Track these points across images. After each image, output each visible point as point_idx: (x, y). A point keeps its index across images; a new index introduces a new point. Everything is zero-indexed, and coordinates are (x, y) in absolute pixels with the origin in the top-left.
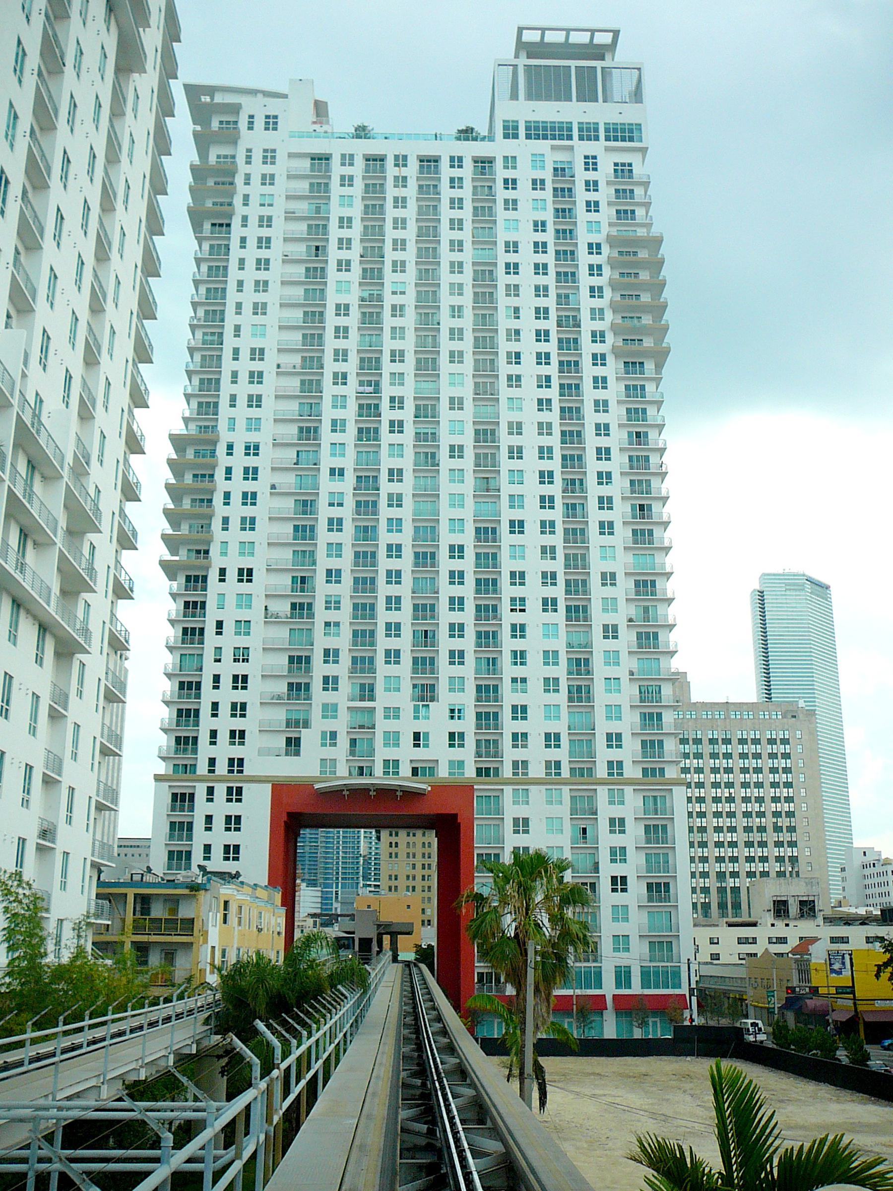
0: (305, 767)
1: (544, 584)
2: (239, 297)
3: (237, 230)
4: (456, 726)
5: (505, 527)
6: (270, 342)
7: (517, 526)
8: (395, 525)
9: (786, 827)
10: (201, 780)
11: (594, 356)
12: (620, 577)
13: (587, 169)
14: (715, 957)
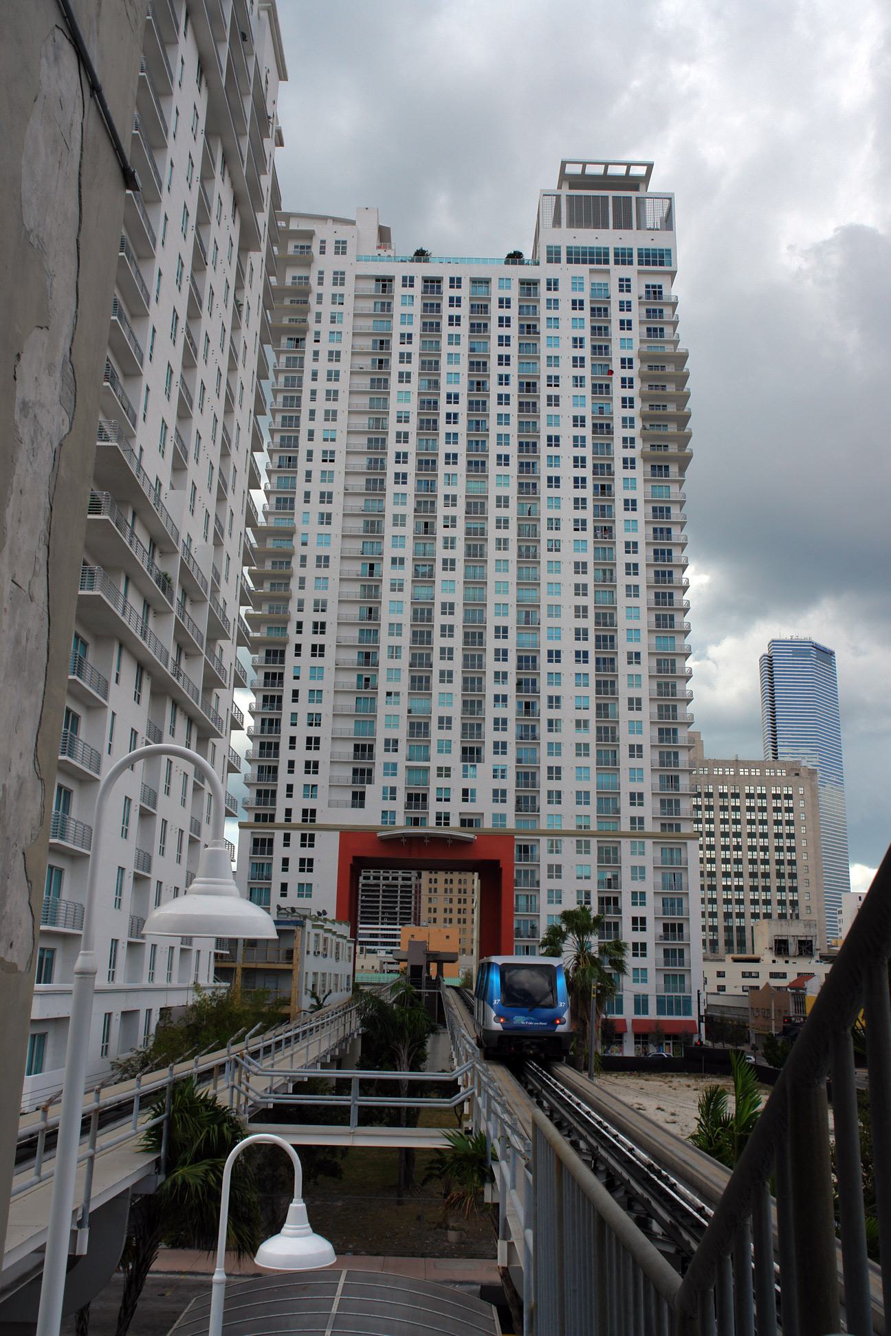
0: (368, 817)
1: (577, 573)
2: (314, 385)
3: (310, 346)
4: (499, 784)
5: (543, 657)
6: (331, 595)
7: (555, 656)
8: (455, 302)
9: (788, 874)
10: (279, 827)
11: (625, 440)
12: (644, 656)
13: (621, 291)
14: (722, 988)
